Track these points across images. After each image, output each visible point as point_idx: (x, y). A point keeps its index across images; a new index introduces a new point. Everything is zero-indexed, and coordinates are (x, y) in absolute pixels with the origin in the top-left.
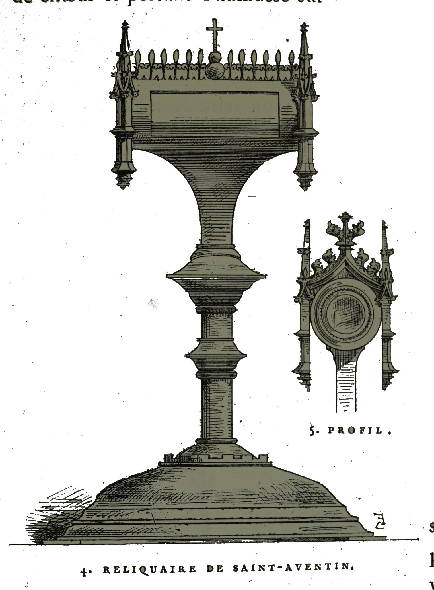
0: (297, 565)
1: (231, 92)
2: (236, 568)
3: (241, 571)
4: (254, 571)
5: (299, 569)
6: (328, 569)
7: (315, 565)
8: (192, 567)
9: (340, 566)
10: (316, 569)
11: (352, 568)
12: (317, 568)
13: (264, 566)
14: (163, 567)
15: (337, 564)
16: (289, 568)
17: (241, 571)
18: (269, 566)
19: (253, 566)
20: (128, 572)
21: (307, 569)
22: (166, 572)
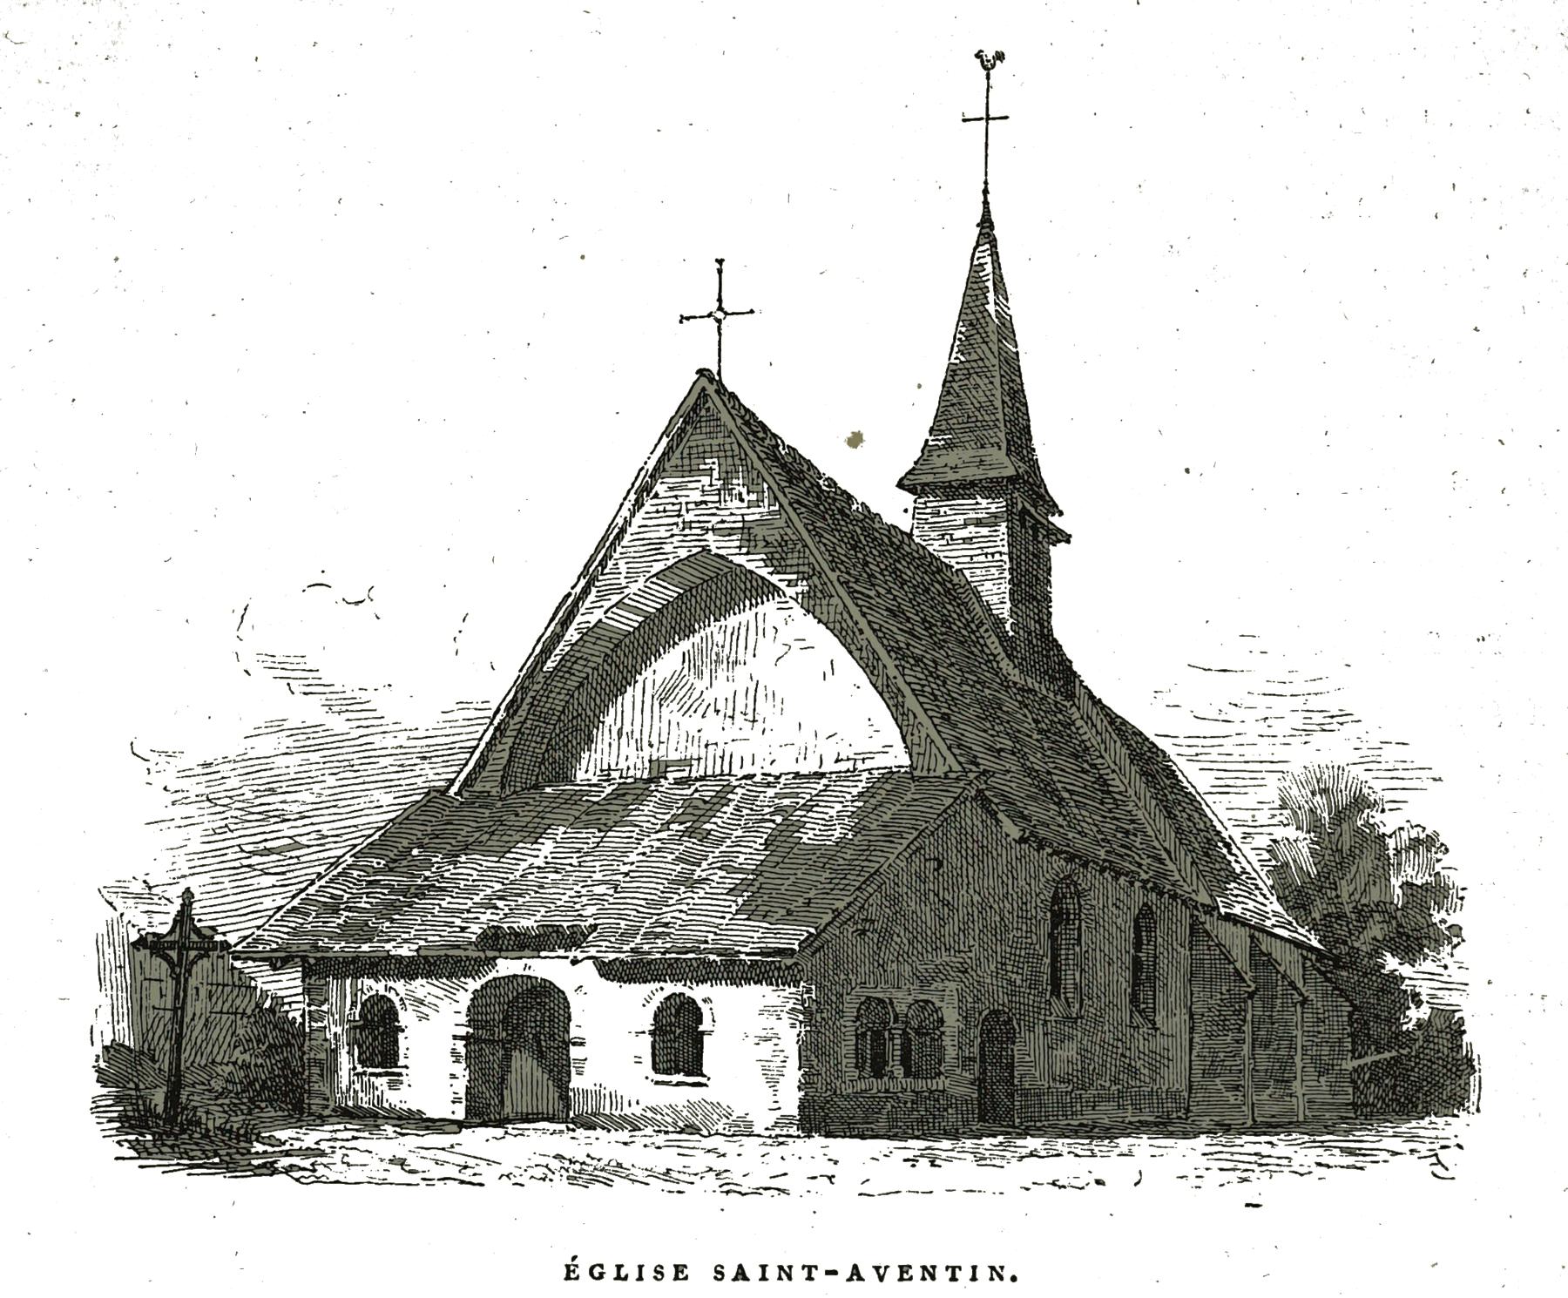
0: (877, 1268)
1: (720, 342)
2: (719, 1273)
3: (848, 1280)
4: (767, 1280)
5: (881, 1278)
6: (810, 1278)
7: (777, 1270)
8: (905, 1269)
9: (983, 1273)
10: (924, 1279)
11: (1014, 1279)
12: (927, 1275)
13: (934, 1267)
14: (855, 1267)
15: (974, 1268)
16: (856, 1274)
17: (848, 1280)
18: (804, 1267)
19: (764, 1267)
20: (626, 1278)
21: (901, 1279)
22: (863, 1280)
